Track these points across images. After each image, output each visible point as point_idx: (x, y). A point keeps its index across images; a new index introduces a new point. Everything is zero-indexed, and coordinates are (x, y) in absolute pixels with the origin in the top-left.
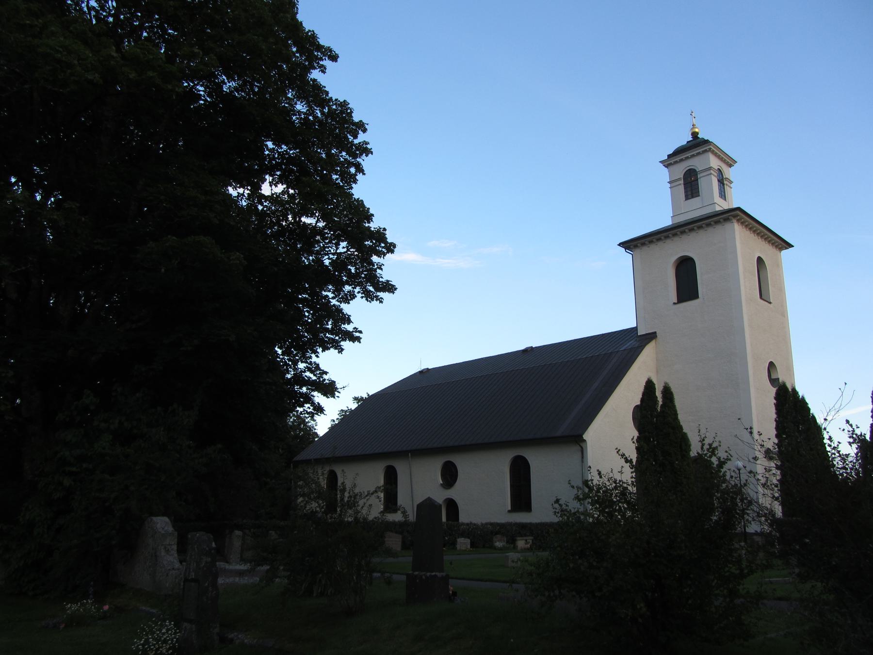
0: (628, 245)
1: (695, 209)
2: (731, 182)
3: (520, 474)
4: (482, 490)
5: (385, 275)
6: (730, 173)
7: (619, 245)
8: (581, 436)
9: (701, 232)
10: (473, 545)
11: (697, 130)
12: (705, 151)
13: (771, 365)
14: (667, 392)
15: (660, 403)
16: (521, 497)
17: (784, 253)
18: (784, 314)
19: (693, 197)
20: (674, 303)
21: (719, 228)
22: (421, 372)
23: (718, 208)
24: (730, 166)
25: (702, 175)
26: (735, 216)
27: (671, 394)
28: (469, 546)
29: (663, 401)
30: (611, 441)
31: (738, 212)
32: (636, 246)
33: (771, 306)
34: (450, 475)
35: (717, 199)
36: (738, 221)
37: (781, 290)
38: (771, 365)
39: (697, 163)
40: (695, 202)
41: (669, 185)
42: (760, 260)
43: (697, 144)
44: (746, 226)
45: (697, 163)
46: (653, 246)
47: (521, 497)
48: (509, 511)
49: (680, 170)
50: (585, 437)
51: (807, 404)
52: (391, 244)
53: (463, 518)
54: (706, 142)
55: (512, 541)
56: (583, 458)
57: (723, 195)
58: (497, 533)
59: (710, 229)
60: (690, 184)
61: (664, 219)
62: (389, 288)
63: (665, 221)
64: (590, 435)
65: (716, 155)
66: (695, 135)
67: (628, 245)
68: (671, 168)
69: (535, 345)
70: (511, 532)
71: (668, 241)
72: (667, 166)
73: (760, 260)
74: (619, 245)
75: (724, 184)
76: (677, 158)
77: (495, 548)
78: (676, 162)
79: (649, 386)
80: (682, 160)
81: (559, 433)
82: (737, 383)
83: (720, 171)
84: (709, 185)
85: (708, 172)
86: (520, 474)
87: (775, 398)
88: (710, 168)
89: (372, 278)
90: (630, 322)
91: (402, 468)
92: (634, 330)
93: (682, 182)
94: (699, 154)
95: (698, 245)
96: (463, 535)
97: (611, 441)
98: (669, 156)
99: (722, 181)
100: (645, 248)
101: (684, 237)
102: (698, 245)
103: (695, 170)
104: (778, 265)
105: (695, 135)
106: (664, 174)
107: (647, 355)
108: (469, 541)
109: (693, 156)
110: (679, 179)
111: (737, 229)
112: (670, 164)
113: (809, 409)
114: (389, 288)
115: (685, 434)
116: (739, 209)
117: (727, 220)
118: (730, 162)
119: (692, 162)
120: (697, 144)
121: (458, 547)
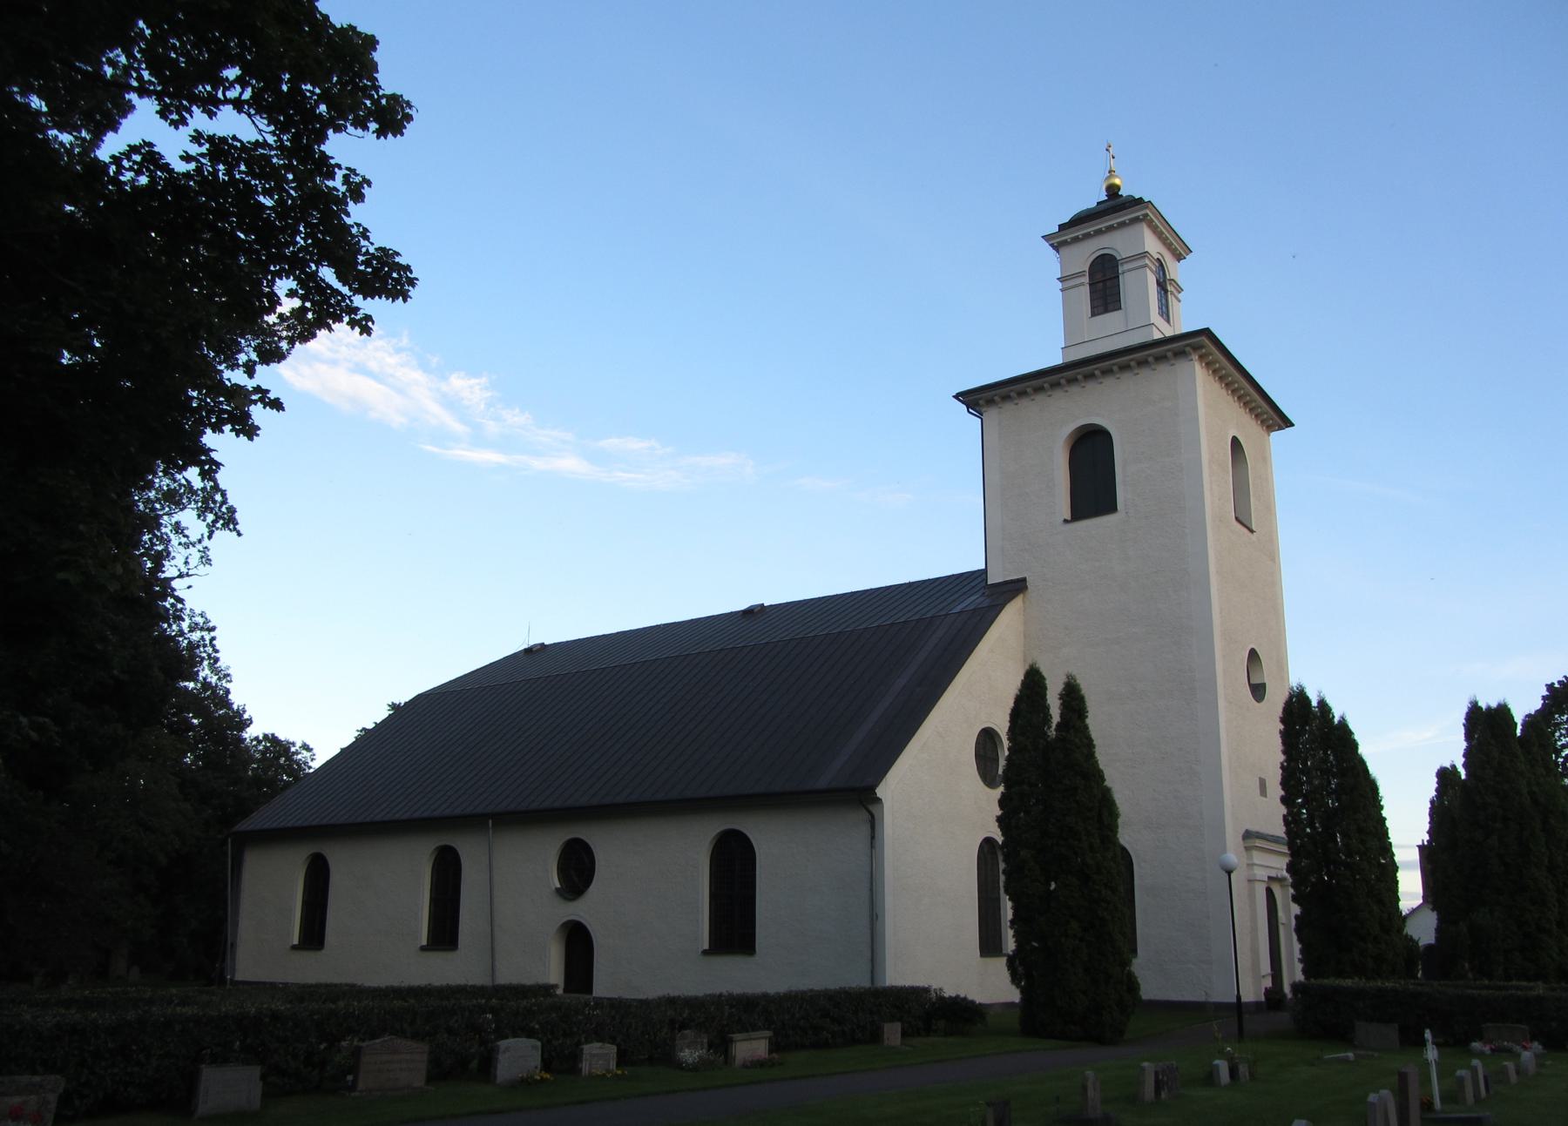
0: (975, 399)
1: (1111, 333)
2: (1180, 290)
3: (733, 870)
4: (649, 908)
5: (378, 221)
6: (1176, 270)
7: (956, 397)
8: (871, 790)
9: (1126, 377)
10: (622, 1059)
11: (1117, 181)
12: (1136, 220)
13: (1253, 655)
14: (1073, 697)
15: (1056, 717)
16: (733, 926)
17: (1276, 436)
18: (1272, 556)
19: (1106, 311)
20: (1066, 521)
21: (1163, 368)
22: (529, 651)
23: (1157, 336)
24: (1179, 257)
25: (1126, 267)
26: (1196, 348)
27: (1081, 699)
28: (613, 1065)
29: (1062, 715)
30: (939, 798)
31: (1204, 339)
32: (991, 402)
33: (1254, 537)
34: (577, 871)
35: (1155, 317)
36: (1201, 357)
37: (1269, 509)
38: (1253, 655)
39: (1118, 243)
40: (1111, 320)
41: (1060, 285)
42: (1236, 443)
43: (1118, 207)
44: (1215, 372)
45: (1118, 243)
46: (1025, 403)
47: (733, 926)
48: (705, 952)
49: (1083, 256)
50: (880, 792)
51: (1351, 733)
52: (395, 99)
53: (604, 985)
54: (1137, 202)
55: (721, 1045)
56: (873, 838)
57: (1165, 312)
58: (683, 1027)
59: (1145, 373)
60: (1104, 286)
61: (1044, 349)
62: (388, 277)
63: (1050, 355)
64: (893, 788)
65: (1155, 230)
66: (1113, 191)
67: (975, 399)
68: (1065, 250)
69: (768, 601)
70: (721, 1018)
71: (1058, 394)
72: (1056, 248)
73: (1236, 443)
74: (956, 397)
75: (1166, 291)
76: (1079, 232)
77: (679, 1065)
78: (1076, 240)
79: (1033, 683)
80: (1087, 236)
81: (822, 783)
82: (1192, 689)
83: (1161, 265)
84: (1138, 287)
85: (1140, 263)
86: (733, 870)
87: (1283, 720)
88: (1145, 254)
89: (340, 245)
90: (972, 560)
91: (471, 852)
92: (982, 574)
93: (1086, 280)
94: (1122, 225)
95: (1112, 407)
96: (598, 1035)
97: (939, 798)
98: (1062, 227)
99: (1162, 285)
100: (1009, 407)
101: (1091, 386)
102: (1112, 407)
103: (1112, 258)
104: (1265, 458)
105: (1113, 191)
106: (1050, 263)
107: (1007, 626)
108: (612, 1050)
109: (1110, 229)
110: (1081, 274)
111: (1199, 378)
112: (1064, 243)
113: (1355, 745)
114: (388, 277)
115: (1108, 791)
116: (1206, 332)
117: (1180, 354)
118: (1180, 251)
119: (1106, 242)
120: (1118, 207)
121: (585, 1067)
